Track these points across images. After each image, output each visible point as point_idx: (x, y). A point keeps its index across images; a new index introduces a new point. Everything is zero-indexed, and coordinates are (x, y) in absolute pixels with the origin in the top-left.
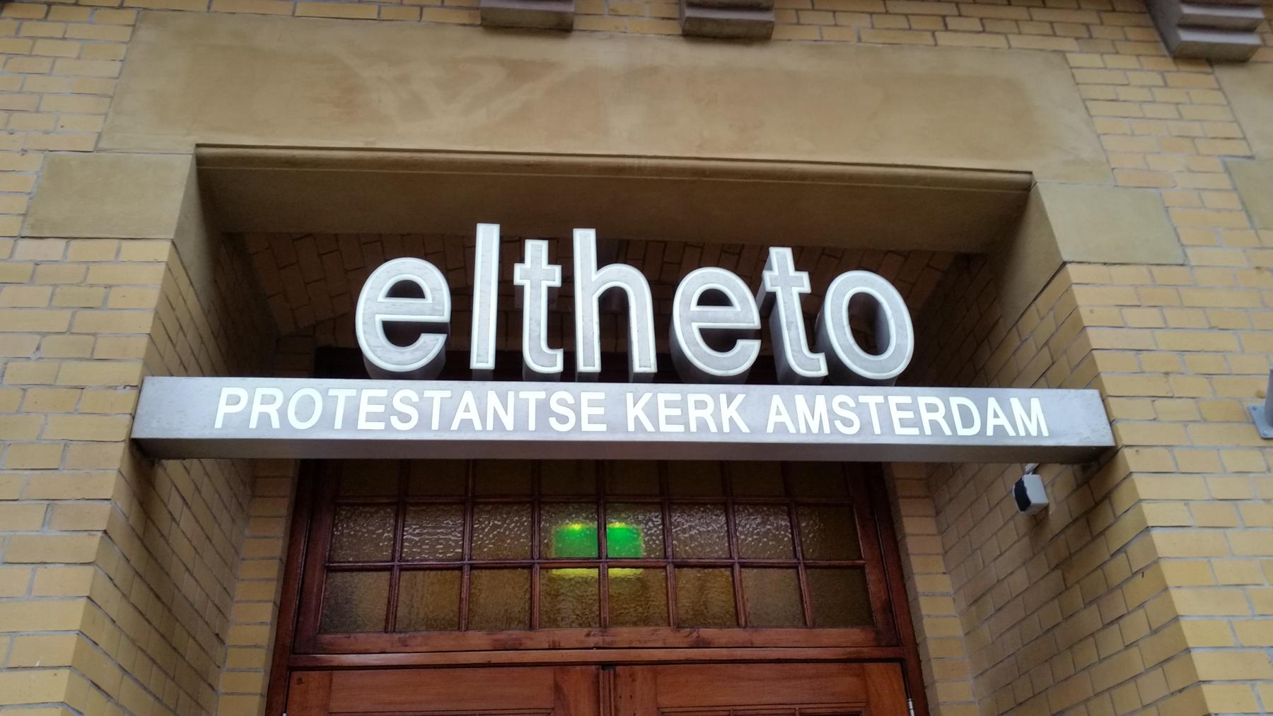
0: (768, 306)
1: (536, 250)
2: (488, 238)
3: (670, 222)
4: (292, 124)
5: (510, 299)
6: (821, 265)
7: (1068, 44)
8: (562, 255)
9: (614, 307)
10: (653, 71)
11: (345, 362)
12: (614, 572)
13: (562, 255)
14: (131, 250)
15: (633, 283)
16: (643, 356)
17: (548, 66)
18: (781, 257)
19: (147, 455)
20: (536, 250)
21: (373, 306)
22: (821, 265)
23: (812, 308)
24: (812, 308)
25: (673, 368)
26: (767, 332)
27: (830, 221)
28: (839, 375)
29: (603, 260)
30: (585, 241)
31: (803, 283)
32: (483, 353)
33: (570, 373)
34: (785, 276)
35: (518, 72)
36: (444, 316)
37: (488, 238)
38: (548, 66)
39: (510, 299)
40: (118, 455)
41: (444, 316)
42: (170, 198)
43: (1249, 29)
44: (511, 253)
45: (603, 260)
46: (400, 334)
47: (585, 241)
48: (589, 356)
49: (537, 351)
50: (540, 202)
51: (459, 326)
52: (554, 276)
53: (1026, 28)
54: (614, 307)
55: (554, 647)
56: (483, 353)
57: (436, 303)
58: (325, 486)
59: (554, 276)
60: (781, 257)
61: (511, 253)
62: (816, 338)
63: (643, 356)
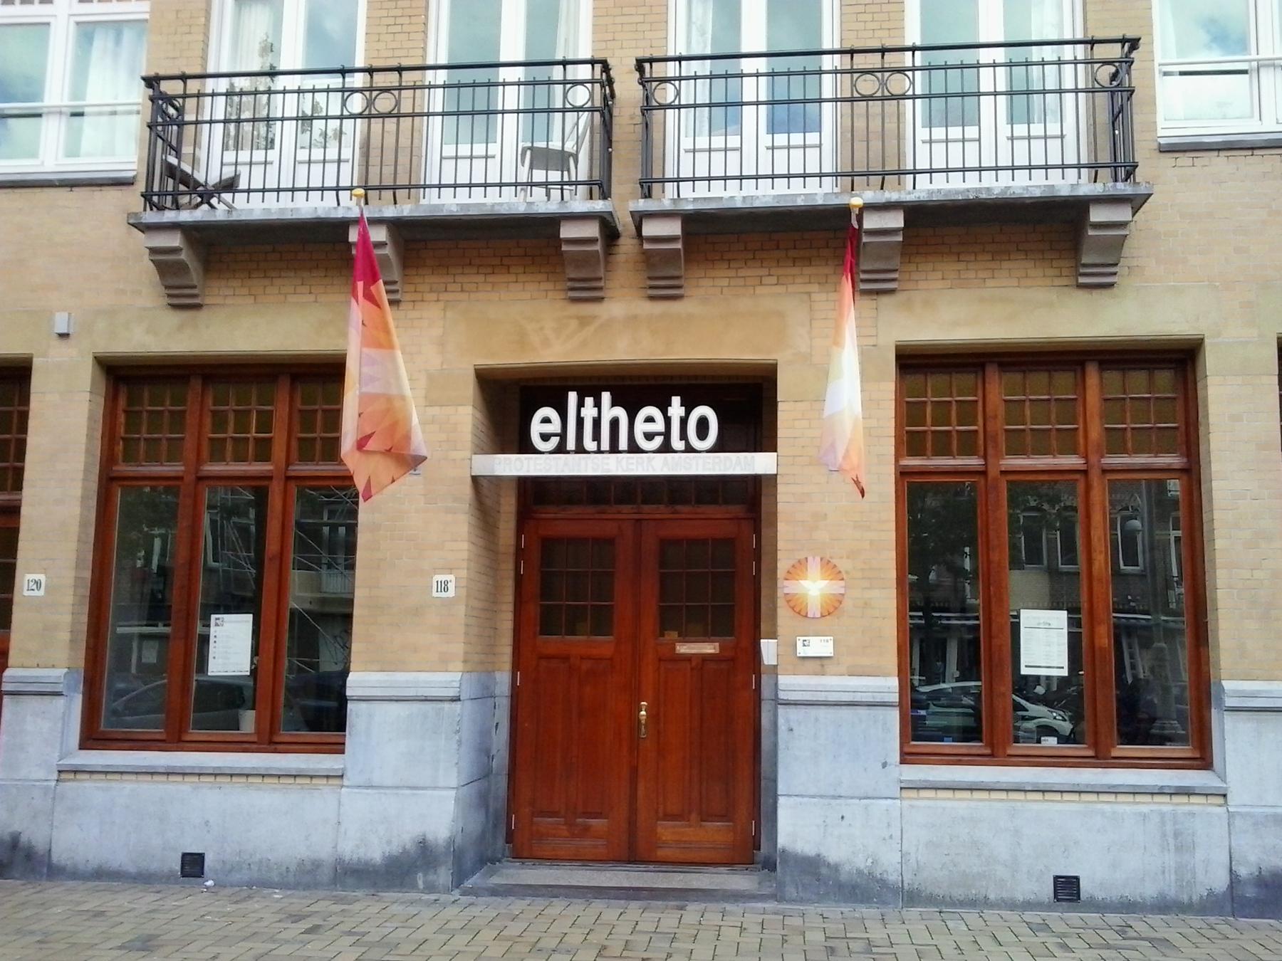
0: (668, 421)
1: (589, 401)
2: (573, 397)
3: (638, 388)
4: (509, 355)
5: (580, 422)
6: (689, 406)
7: (815, 288)
8: (598, 404)
9: (615, 423)
10: (635, 317)
11: (526, 447)
12: (156, 189)
13: (598, 404)
14: (460, 408)
15: (621, 413)
16: (623, 443)
17: (595, 317)
18: (676, 400)
19: (475, 479)
20: (589, 401)
21: (536, 428)
22: (689, 406)
23: (684, 422)
24: (684, 422)
25: (634, 448)
26: (667, 434)
27: (695, 384)
28: (689, 449)
29: (614, 404)
30: (606, 397)
31: (682, 411)
32: (571, 444)
33: (599, 451)
34: (676, 409)
35: (584, 321)
36: (559, 431)
37: (573, 397)
38: (595, 317)
39: (580, 422)
40: (469, 480)
41: (559, 431)
42: (469, 388)
43: (894, 280)
44: (581, 404)
45: (614, 404)
46: (545, 437)
47: (606, 397)
48: (605, 445)
49: (589, 444)
50: (591, 382)
51: (563, 436)
52: (594, 412)
53: (799, 280)
54: (615, 423)
55: (619, 512)
56: (571, 444)
57: (555, 427)
58: (534, 492)
59: (594, 412)
60: (676, 400)
61: (581, 404)
62: (683, 435)
63: (623, 443)
